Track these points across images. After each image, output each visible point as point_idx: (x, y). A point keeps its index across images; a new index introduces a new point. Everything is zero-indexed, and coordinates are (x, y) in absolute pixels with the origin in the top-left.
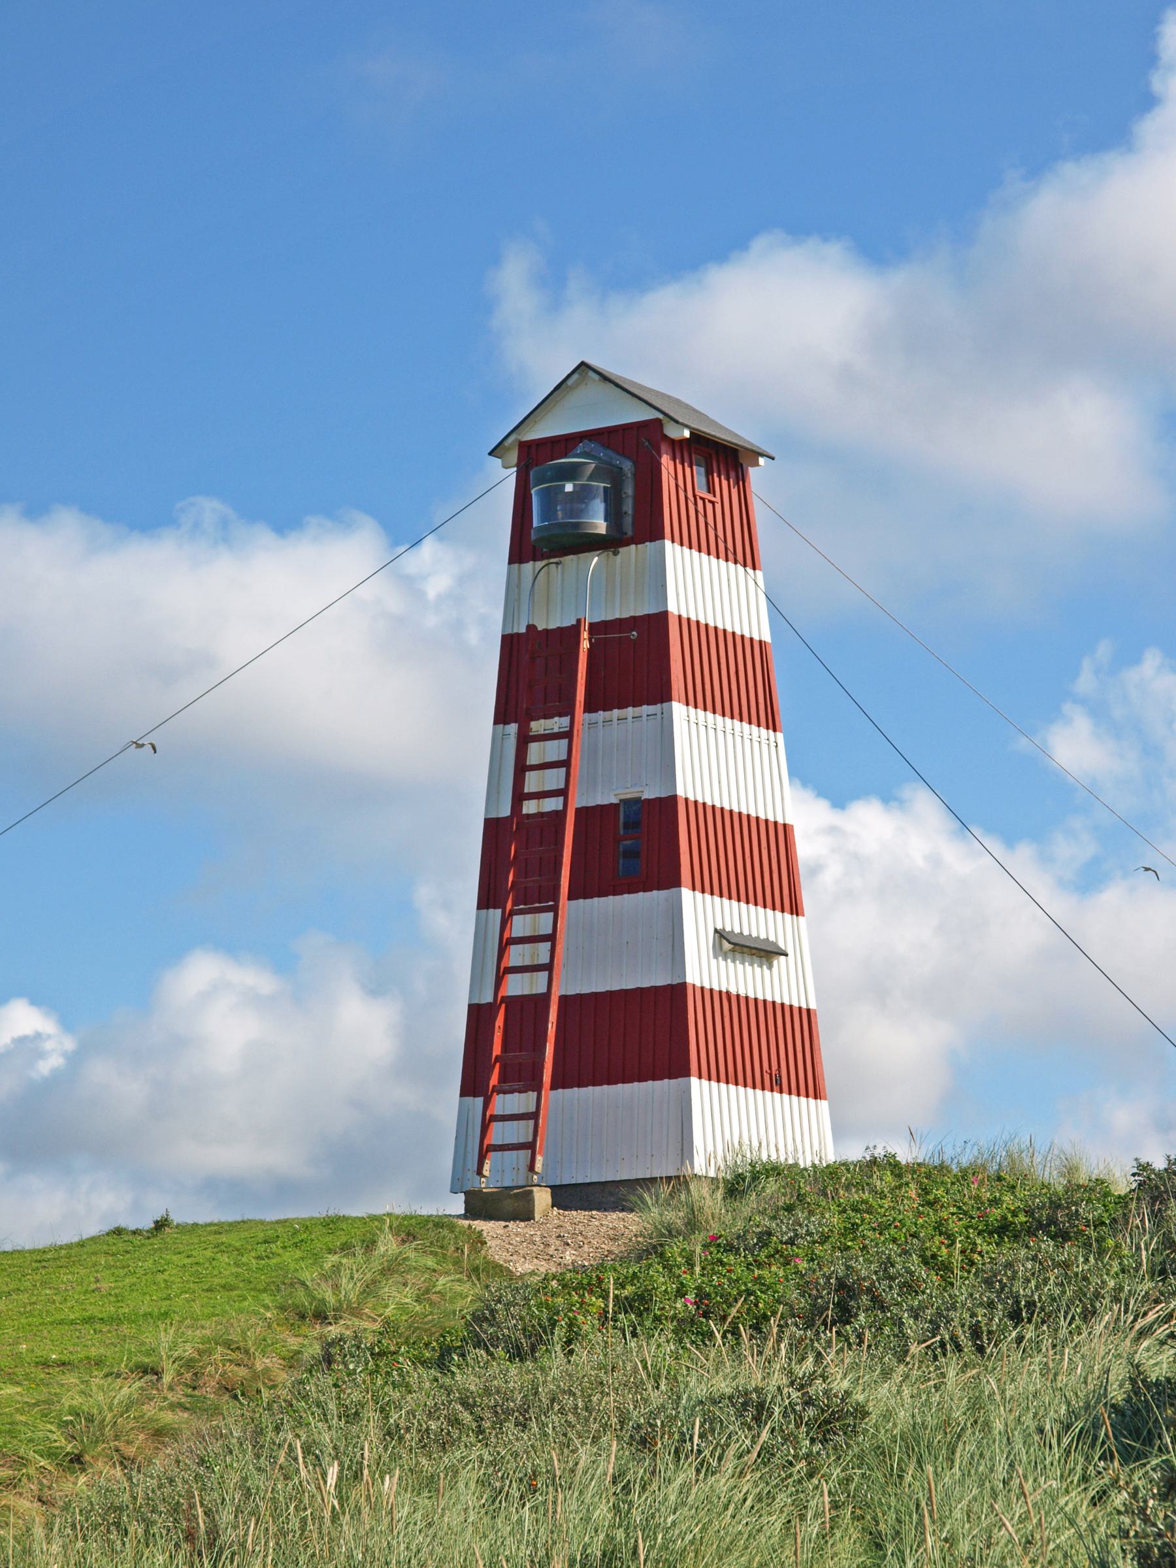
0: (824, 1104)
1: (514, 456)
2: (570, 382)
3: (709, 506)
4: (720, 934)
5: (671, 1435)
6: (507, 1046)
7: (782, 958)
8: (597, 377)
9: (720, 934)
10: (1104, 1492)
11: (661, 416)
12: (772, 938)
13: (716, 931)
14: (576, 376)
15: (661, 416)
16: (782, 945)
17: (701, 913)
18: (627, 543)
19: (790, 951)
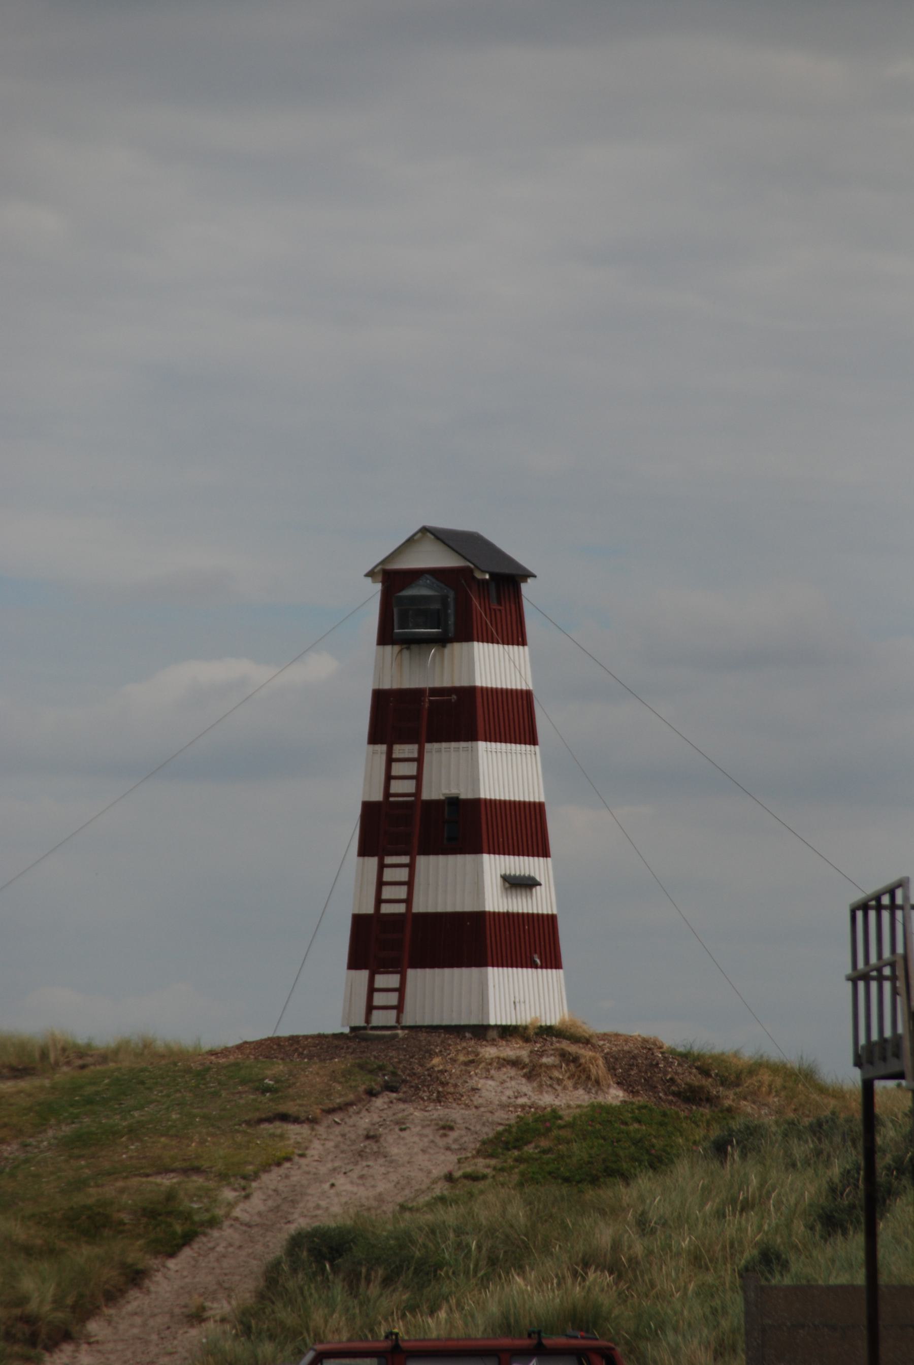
0: (561, 971)
1: (380, 578)
2: (416, 538)
3: (498, 613)
4: (505, 879)
5: (734, 1225)
6: (385, 943)
7: (538, 887)
8: (432, 537)
9: (505, 879)
10: (220, 1175)
11: (472, 566)
12: (532, 874)
13: (502, 877)
14: (420, 535)
15: (472, 566)
16: (538, 879)
17: (494, 866)
18: (452, 641)
19: (542, 882)
